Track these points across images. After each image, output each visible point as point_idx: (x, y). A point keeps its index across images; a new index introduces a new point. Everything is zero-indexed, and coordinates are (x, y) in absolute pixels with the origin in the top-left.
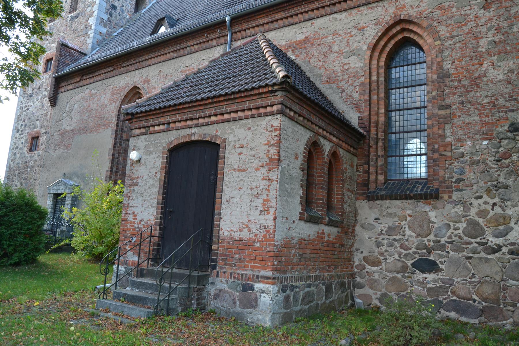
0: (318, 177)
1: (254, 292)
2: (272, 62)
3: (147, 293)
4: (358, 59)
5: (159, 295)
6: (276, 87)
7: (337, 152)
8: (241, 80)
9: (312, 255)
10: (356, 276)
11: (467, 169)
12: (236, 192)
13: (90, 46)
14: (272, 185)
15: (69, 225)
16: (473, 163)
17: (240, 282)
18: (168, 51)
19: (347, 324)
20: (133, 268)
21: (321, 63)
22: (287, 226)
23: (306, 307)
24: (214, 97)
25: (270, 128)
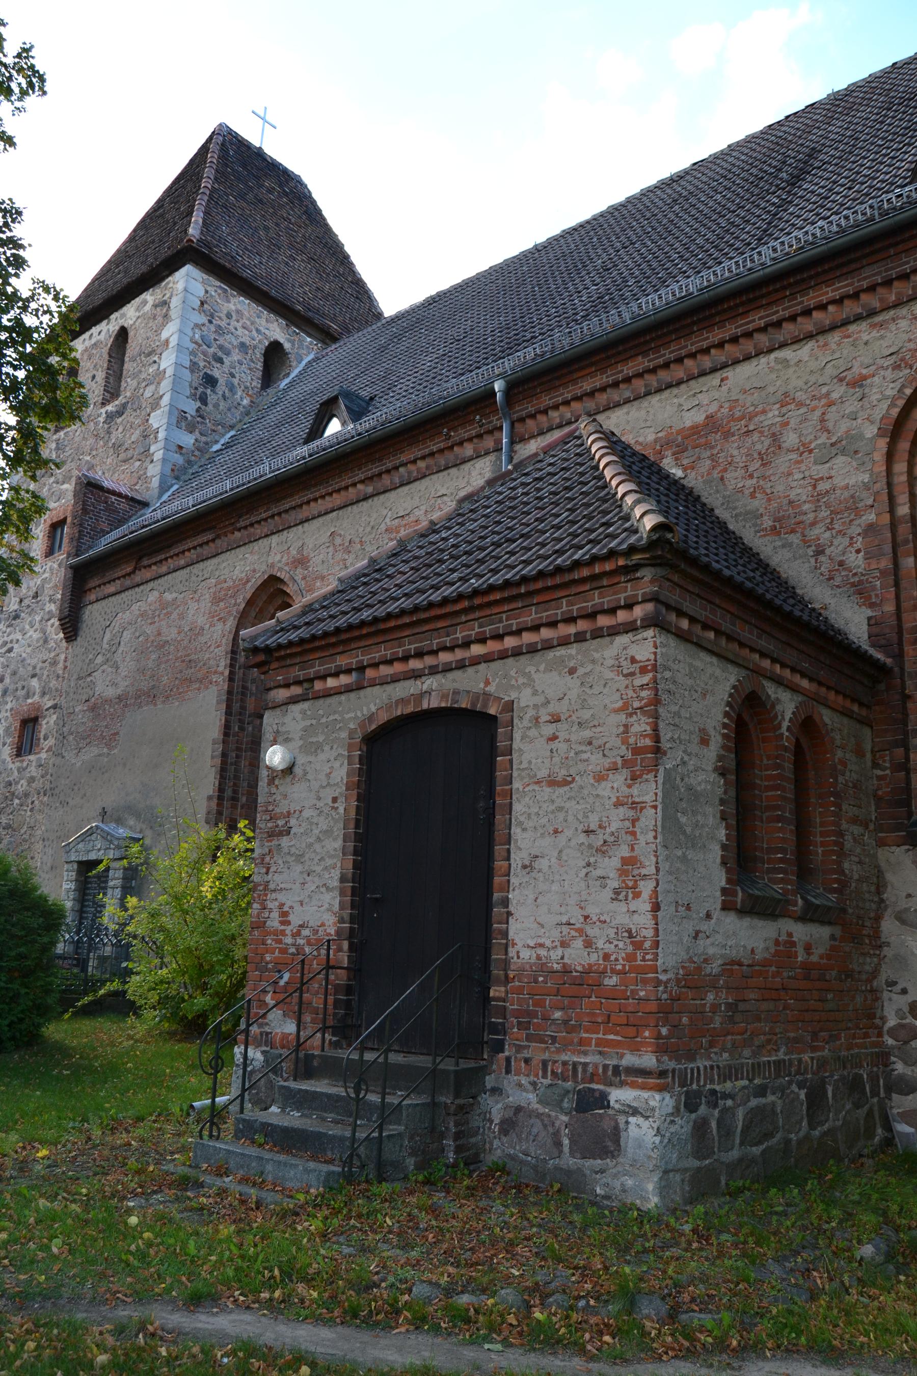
0: (768, 789)
1: (610, 1112)
2: (621, 490)
3: (324, 1119)
4: (854, 463)
5: (355, 1127)
6: (637, 557)
7: (816, 717)
8: (543, 545)
9: (765, 1006)
10: (893, 1059)
12: (548, 840)
13: (155, 482)
14: (643, 819)
15: (120, 941)
17: (569, 1085)
18: (350, 481)
19: (875, 1196)
20: (285, 1052)
21: (754, 481)
22: (689, 927)
23: (756, 1150)
24: (476, 592)
25: (627, 668)
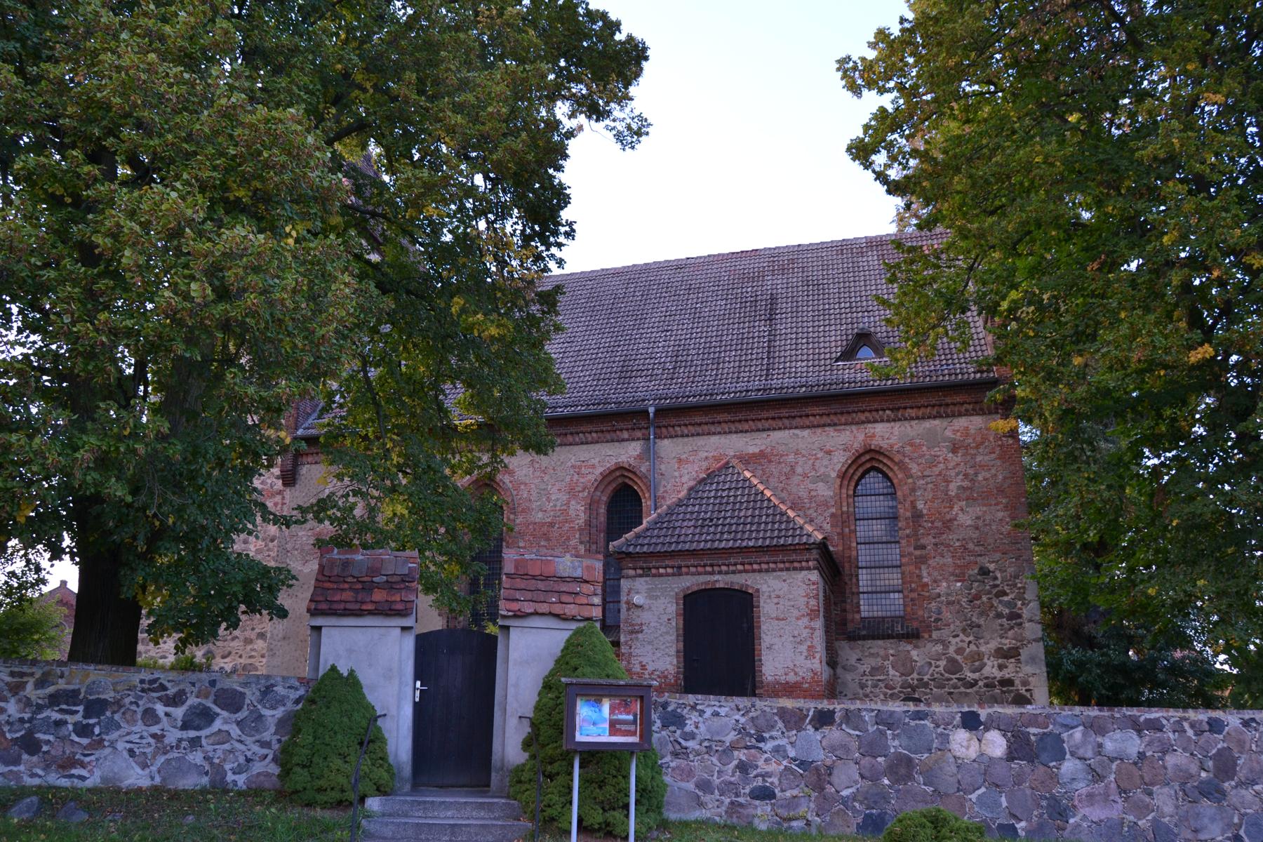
11: (944, 608)
16: (949, 603)
